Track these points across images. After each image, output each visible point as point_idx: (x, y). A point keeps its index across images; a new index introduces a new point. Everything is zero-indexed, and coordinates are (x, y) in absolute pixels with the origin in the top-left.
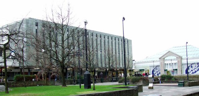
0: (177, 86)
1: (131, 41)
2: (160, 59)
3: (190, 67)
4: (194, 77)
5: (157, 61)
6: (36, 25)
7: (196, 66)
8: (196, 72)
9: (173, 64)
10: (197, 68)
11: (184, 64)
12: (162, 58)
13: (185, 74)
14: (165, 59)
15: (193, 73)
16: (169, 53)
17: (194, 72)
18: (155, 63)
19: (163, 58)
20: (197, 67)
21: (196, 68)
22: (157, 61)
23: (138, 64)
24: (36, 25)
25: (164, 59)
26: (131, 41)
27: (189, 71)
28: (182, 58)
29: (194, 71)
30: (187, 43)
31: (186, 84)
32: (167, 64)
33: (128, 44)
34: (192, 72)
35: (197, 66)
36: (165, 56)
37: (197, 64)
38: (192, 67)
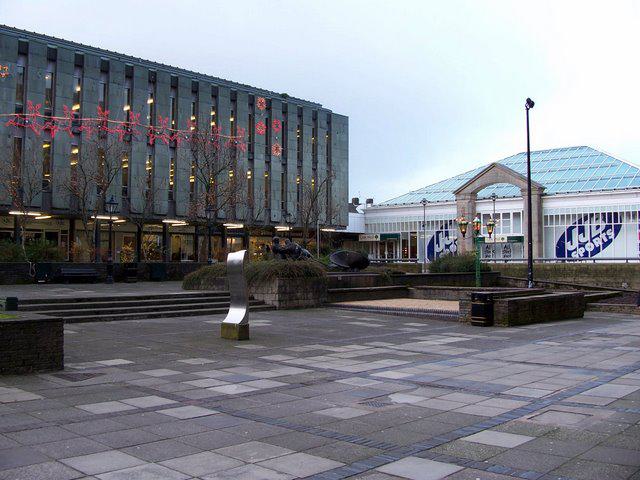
0: (455, 320)
1: (344, 120)
2: (457, 193)
3: (575, 232)
4: (584, 271)
5: (444, 204)
6: (20, 53)
7: (598, 227)
8: (597, 250)
9: (497, 216)
10: (603, 236)
11: (557, 216)
12: (469, 191)
13: (555, 257)
14: (481, 194)
15: (586, 254)
16: (494, 173)
17: (589, 250)
18: (429, 212)
19: (470, 189)
20: (600, 230)
21: (598, 236)
22: (444, 204)
23: (378, 215)
24: (20, 53)
25: (474, 194)
26: (344, 120)
27: (568, 246)
28: (545, 192)
29: (590, 247)
30: (530, 103)
31: (501, 307)
32: (506, 215)
33: (330, 128)
34: (581, 251)
35: (603, 225)
36: (477, 184)
37: (604, 219)
38: (582, 230)
